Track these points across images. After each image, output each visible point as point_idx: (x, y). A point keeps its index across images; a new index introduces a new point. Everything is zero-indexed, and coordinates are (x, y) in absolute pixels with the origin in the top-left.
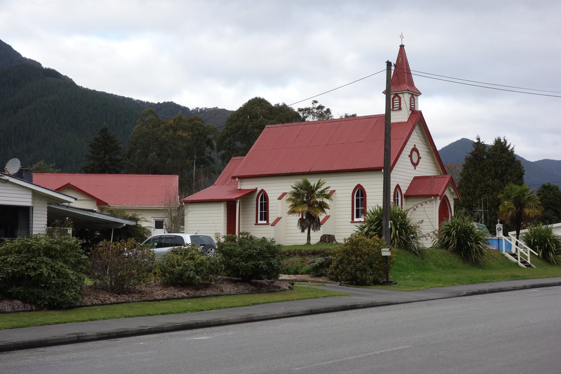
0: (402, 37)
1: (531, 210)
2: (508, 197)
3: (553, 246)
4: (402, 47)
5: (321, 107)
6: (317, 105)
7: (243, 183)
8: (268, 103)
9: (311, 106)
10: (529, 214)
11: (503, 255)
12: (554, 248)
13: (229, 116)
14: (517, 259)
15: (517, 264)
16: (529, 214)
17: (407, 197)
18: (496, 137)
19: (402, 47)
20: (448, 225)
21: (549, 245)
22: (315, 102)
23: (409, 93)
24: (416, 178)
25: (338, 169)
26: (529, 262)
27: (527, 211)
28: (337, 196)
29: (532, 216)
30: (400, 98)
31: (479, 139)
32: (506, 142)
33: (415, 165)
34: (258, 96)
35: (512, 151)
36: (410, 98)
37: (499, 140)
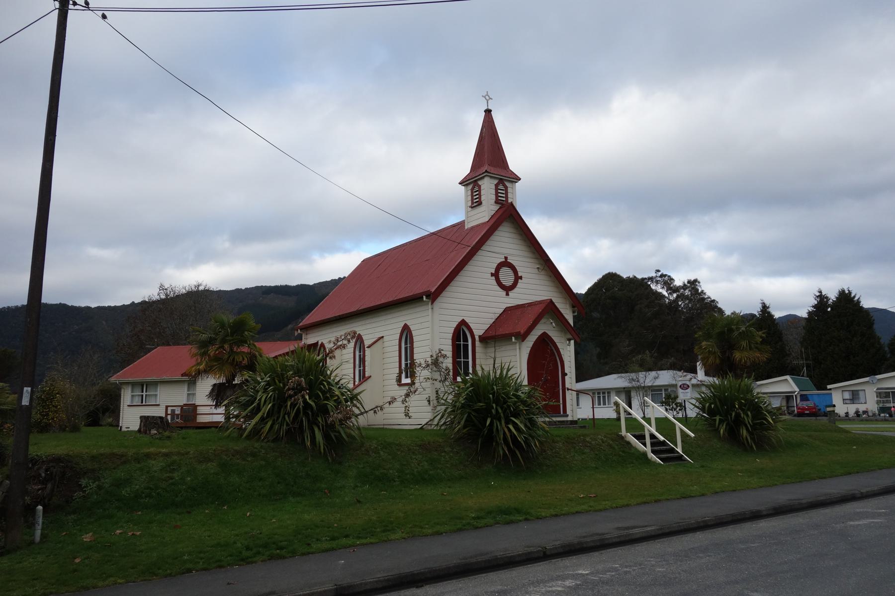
0: (487, 98)
1: (746, 354)
2: (708, 336)
3: (747, 416)
4: (488, 112)
5: (662, 276)
6: (660, 274)
7: (309, 336)
8: (619, 276)
9: (654, 275)
10: (741, 360)
11: (622, 438)
12: (748, 419)
13: (804, 323)
14: (645, 444)
15: (645, 454)
16: (741, 360)
17: (484, 339)
18: (840, 288)
19: (488, 112)
20: (268, 384)
21: (738, 415)
22: (658, 271)
23: (491, 177)
24: (507, 310)
25: (383, 301)
26: (679, 450)
27: (737, 355)
28: (386, 344)
29: (745, 362)
30: (480, 187)
31: (820, 292)
32: (850, 293)
33: (508, 289)
34: (611, 271)
35: (858, 302)
36: (497, 186)
37: (843, 291)
